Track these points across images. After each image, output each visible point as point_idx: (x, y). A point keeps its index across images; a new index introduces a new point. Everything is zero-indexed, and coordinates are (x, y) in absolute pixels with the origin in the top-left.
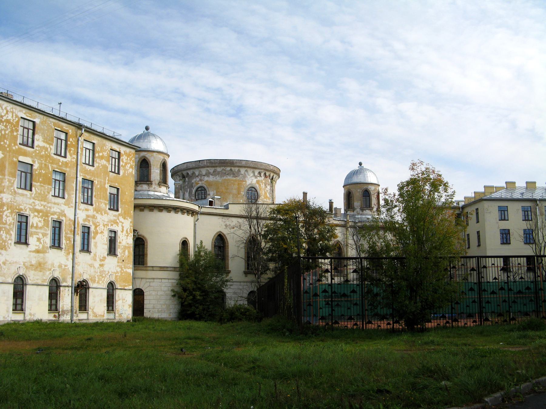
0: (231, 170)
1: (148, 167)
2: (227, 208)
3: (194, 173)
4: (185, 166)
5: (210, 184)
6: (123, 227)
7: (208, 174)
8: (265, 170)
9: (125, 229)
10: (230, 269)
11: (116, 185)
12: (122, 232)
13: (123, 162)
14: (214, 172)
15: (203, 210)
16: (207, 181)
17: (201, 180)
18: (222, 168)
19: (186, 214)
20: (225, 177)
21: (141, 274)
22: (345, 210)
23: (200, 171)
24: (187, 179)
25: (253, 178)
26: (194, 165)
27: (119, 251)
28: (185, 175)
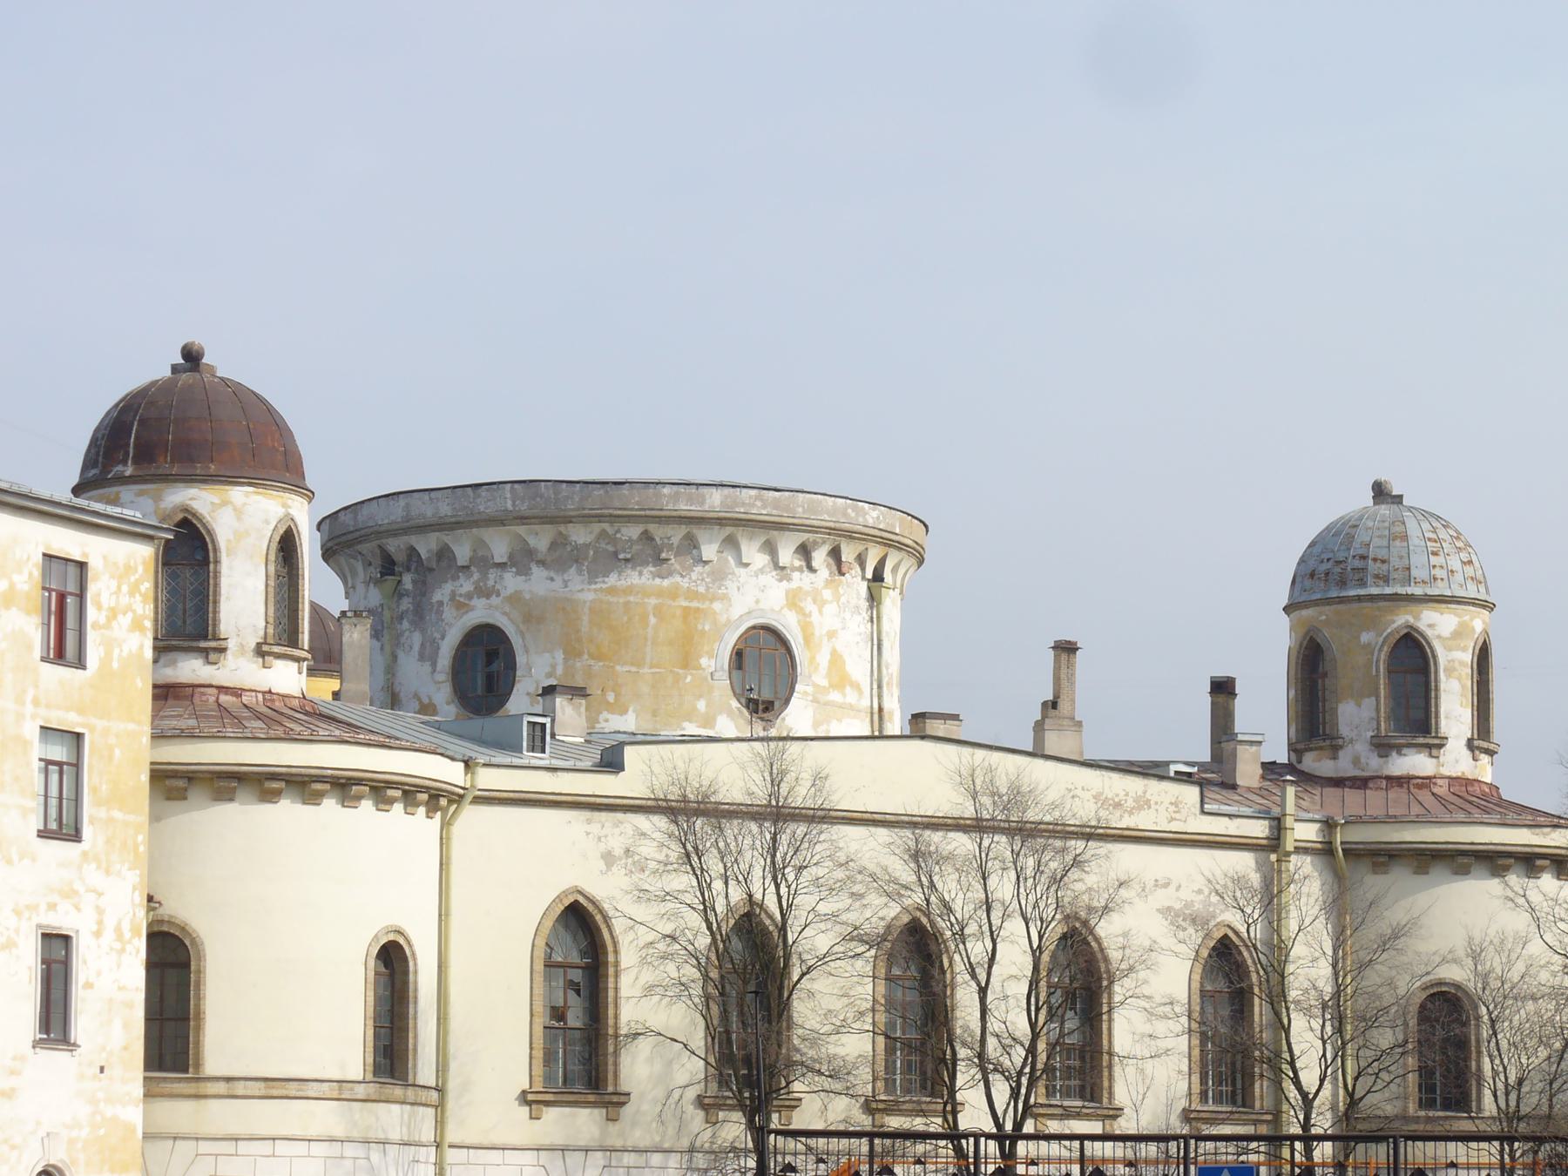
0: (647, 537)
1: (206, 562)
2: (611, 762)
3: (444, 554)
4: (396, 512)
5: (532, 615)
6: (100, 911)
7: (522, 560)
8: (832, 531)
9: (110, 924)
10: (624, 1088)
11: (72, 721)
12: (98, 934)
13: (99, 607)
14: (553, 546)
15: (490, 779)
16: (515, 599)
17: (484, 592)
18: (597, 527)
19: (398, 807)
20: (612, 580)
21: (179, 1114)
22: (1292, 747)
23: (481, 543)
24: (408, 581)
25: (770, 578)
26: (445, 509)
27: (81, 1026)
28: (400, 557)
